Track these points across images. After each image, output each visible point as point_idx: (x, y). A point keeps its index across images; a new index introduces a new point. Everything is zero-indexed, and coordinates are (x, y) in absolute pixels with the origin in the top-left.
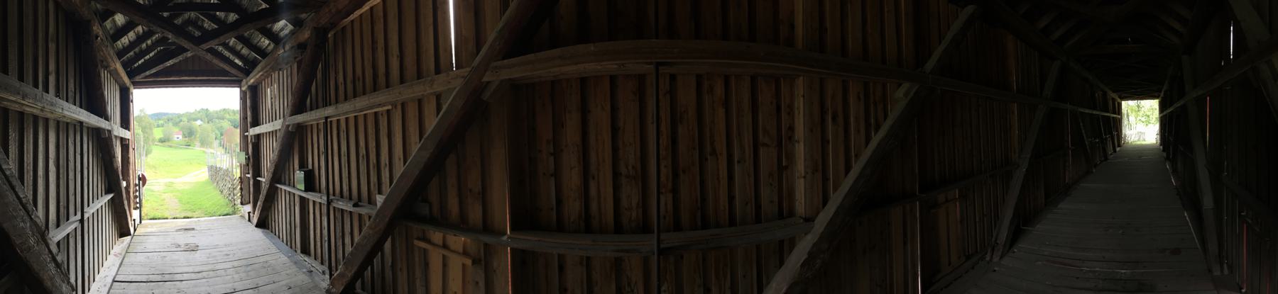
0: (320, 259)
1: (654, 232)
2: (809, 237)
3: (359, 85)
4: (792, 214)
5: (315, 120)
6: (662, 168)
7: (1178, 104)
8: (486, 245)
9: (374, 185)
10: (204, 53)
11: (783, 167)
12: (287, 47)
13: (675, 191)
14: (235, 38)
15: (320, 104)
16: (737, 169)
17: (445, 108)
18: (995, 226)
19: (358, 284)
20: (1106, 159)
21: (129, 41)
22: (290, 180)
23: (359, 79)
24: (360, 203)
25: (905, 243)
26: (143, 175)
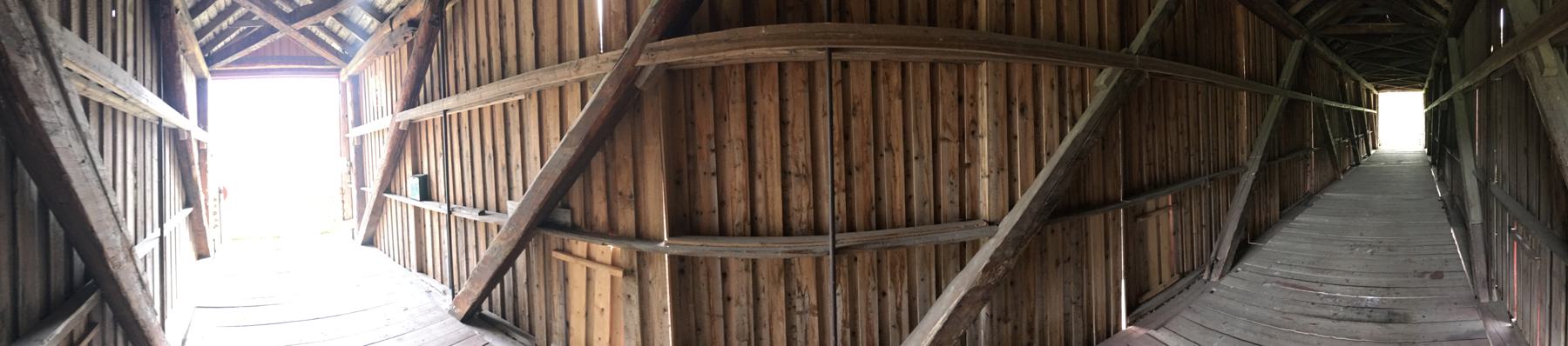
2: (992, 241)
3: (485, 71)
4: (975, 216)
5: (428, 115)
7: (1444, 98)
8: (640, 253)
9: (504, 190)
10: (297, 34)
11: (965, 166)
12: (396, 24)
13: (848, 190)
14: (333, 16)
15: (437, 94)
17: (592, 98)
18: (1216, 240)
19: (485, 305)
20: (1358, 164)
21: (209, 17)
22: (401, 189)
23: (484, 64)
24: (486, 212)
25: (1107, 257)
26: (224, 188)
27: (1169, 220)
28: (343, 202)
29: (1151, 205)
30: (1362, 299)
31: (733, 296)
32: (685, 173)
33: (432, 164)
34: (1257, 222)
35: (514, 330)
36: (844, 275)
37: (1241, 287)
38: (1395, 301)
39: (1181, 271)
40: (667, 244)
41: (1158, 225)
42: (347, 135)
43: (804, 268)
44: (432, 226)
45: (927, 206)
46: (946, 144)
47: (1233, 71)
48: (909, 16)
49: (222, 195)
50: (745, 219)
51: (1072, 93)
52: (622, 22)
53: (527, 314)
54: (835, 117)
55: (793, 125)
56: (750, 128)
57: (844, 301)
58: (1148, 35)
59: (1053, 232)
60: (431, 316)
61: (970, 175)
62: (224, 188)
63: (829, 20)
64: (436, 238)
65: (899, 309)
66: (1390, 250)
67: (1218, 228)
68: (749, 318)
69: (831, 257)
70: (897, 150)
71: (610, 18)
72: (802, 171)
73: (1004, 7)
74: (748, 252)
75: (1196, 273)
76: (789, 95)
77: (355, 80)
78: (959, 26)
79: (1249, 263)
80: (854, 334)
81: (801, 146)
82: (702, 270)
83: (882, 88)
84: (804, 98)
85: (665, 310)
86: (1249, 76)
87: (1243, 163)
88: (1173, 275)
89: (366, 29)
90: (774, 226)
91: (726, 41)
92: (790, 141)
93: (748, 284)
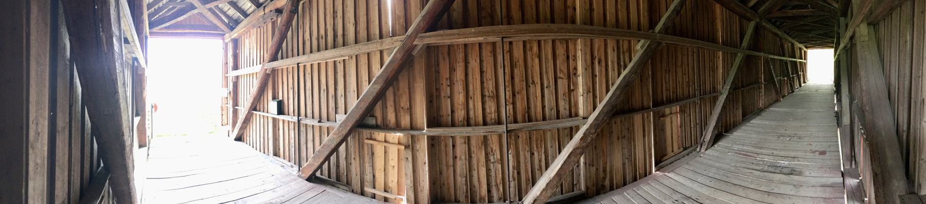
0: (288, 158)
1: (504, 124)
3: (322, 42)
4: (577, 115)
6: (507, 92)
8: (412, 137)
9: (332, 109)
11: (571, 91)
12: (267, 10)
13: (514, 103)
16: (546, 91)
23: (322, 38)
25: (644, 136)
26: (155, 105)
27: (677, 120)
28: (222, 115)
29: (667, 111)
30: (779, 163)
31: (458, 156)
32: (435, 97)
33: (286, 93)
34: (728, 123)
35: (338, 184)
36: (513, 144)
37: (716, 154)
38: (796, 164)
39: (684, 146)
40: (427, 131)
41: (672, 122)
42: (227, 75)
43: (494, 141)
44: (283, 129)
45: (553, 111)
46: (561, 80)
47: (714, 40)
48: (542, 17)
49: (153, 109)
50: (464, 118)
51: (624, 53)
52: (402, 20)
53: (345, 174)
54: (506, 69)
55: (486, 73)
56: (466, 75)
57: (513, 157)
58: (664, 24)
59: (615, 123)
60: (288, 179)
61: (574, 95)
62: (155, 105)
63: (502, 25)
64: (287, 137)
65: (540, 161)
66: (800, 139)
67: (706, 124)
68: (466, 166)
69: (505, 133)
70: (537, 84)
71: (395, 19)
72: (491, 94)
73: (589, 11)
74: (466, 133)
75: (693, 148)
76: (484, 59)
77: (236, 42)
78: (566, 22)
79: (722, 143)
80: (519, 173)
81: (490, 83)
82: (443, 144)
83: (528, 53)
84: (491, 60)
85: (425, 163)
86: (724, 43)
87: (720, 90)
88: (679, 149)
89: (246, 11)
90: (478, 121)
91: (457, 34)
92: (485, 80)
93: (465, 150)
